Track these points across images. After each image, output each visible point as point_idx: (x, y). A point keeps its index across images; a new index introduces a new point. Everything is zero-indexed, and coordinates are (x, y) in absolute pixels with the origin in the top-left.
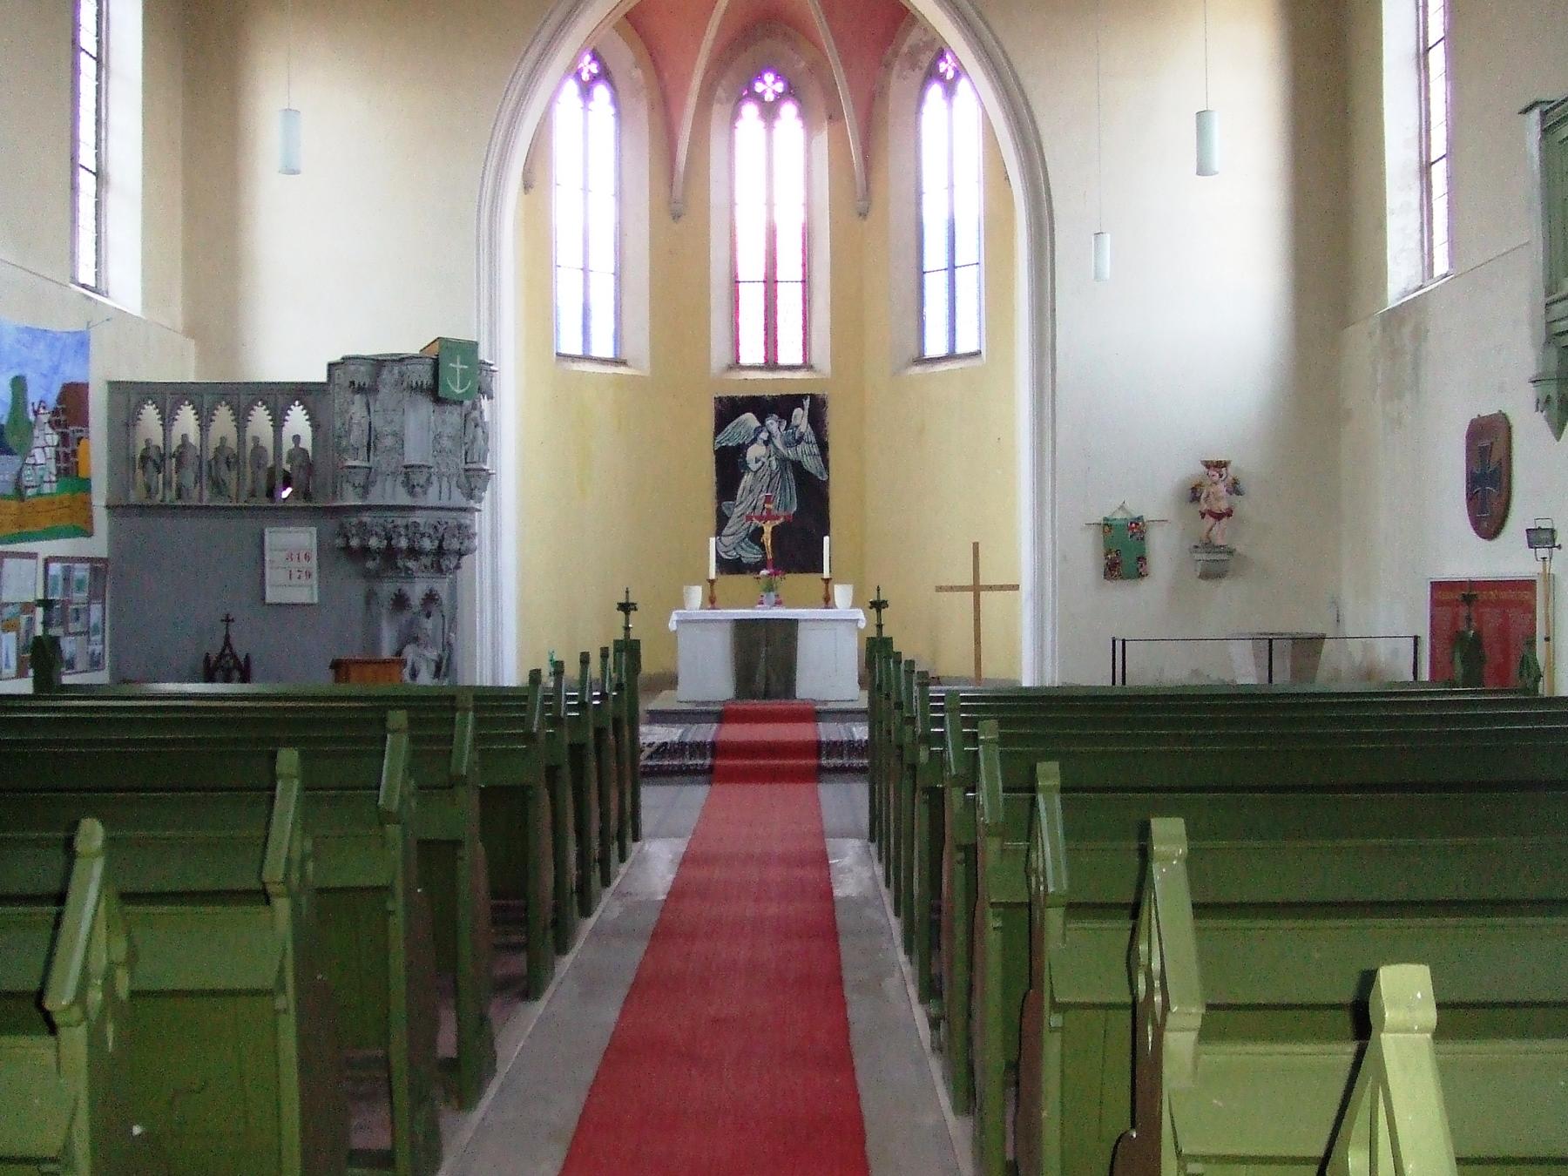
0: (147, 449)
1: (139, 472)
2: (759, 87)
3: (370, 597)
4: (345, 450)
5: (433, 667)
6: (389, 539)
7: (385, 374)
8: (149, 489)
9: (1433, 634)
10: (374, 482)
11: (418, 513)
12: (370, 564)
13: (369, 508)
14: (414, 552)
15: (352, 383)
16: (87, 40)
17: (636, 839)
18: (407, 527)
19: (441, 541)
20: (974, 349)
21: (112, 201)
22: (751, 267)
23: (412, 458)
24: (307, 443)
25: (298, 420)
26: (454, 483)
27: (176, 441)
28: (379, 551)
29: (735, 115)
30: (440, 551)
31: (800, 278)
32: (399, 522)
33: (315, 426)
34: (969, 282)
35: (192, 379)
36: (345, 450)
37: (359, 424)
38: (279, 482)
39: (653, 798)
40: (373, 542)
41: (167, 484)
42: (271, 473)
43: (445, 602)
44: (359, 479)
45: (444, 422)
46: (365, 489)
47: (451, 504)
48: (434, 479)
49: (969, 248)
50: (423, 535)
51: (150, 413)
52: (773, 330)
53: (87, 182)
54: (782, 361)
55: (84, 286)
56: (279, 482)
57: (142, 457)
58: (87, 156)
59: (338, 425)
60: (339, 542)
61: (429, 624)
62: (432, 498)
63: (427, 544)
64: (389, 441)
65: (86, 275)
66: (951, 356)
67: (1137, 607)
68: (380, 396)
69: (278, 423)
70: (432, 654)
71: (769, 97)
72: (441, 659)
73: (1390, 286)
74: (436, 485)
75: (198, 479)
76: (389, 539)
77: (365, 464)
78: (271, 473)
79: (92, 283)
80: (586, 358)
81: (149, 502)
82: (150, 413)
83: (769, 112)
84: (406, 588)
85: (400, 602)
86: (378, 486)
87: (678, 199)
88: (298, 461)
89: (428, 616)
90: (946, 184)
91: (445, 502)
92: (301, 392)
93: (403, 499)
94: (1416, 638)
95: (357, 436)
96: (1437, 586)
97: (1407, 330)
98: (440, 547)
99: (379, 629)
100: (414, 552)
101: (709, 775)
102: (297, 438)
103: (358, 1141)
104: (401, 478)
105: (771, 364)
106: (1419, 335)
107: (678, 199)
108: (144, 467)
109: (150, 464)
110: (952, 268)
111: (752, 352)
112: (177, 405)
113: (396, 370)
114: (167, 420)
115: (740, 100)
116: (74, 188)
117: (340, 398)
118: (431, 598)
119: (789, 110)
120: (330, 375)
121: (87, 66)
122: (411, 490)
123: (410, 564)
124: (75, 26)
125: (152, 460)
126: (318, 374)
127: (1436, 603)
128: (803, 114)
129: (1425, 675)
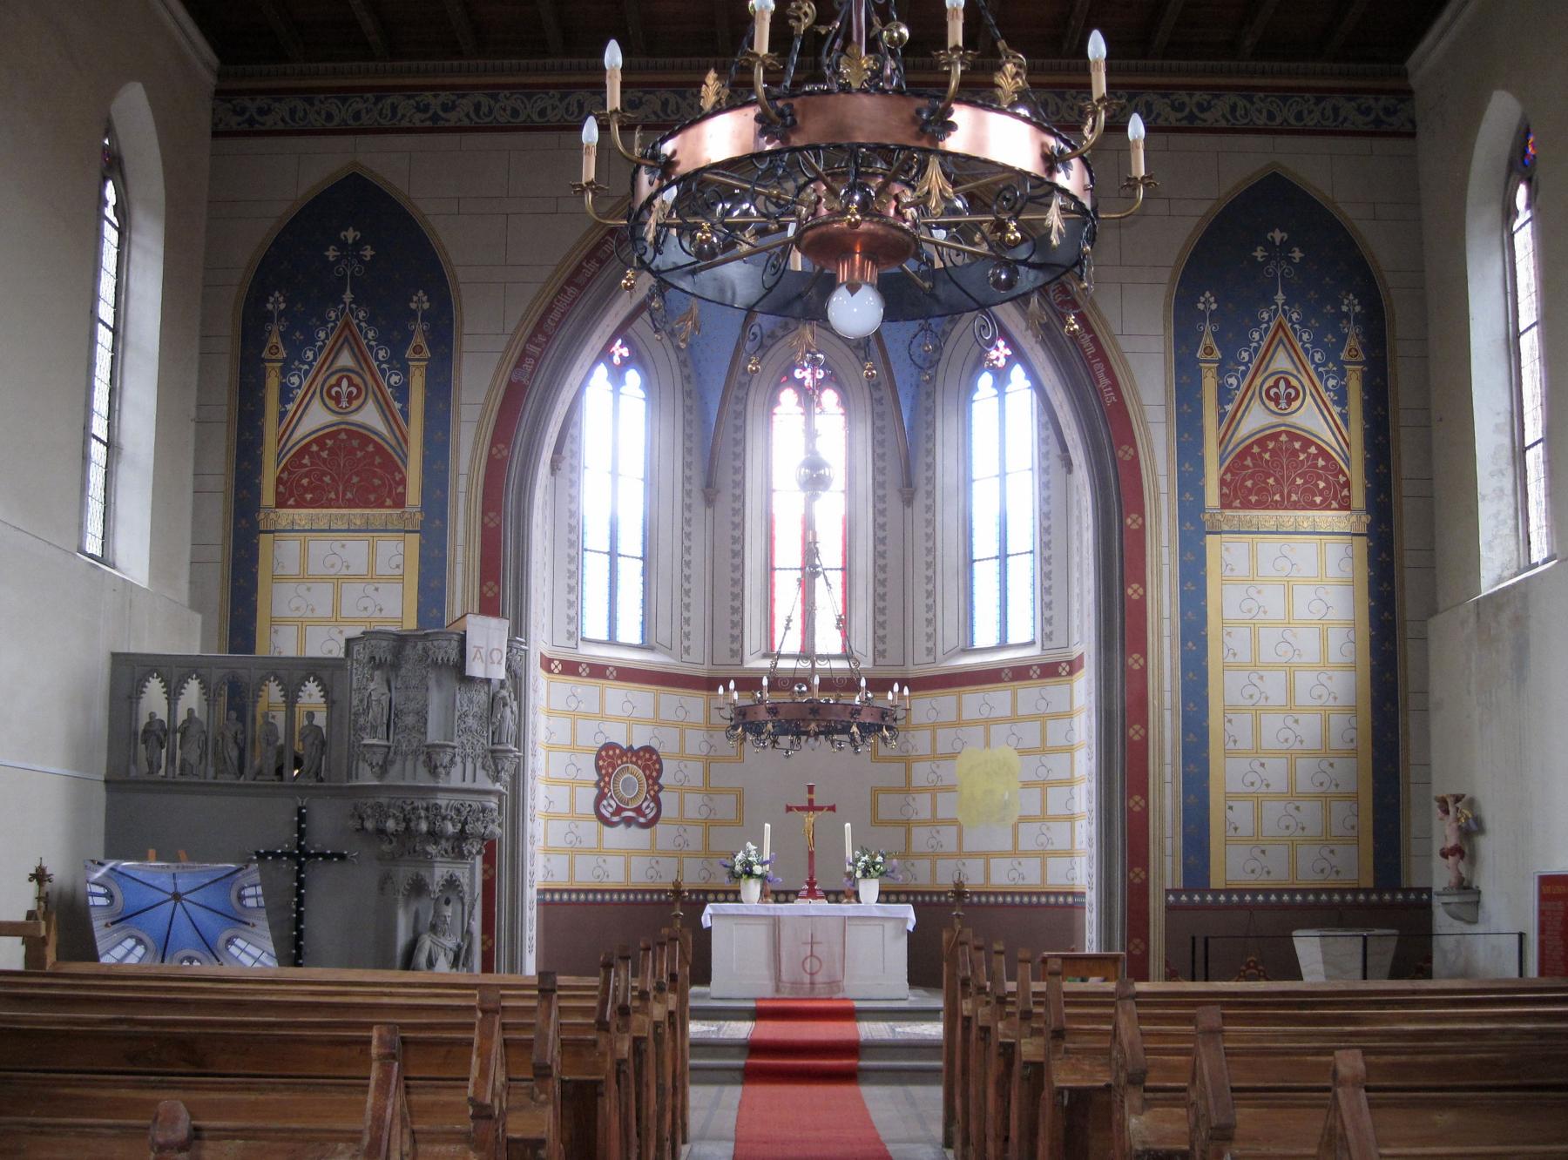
0: (149, 724)
1: (142, 747)
2: (798, 374)
3: (385, 881)
4: (363, 729)
5: (451, 956)
6: (407, 821)
7: (409, 651)
8: (150, 764)
9: (1542, 929)
10: (393, 762)
11: (440, 795)
12: (386, 847)
13: (388, 788)
14: (434, 835)
15: (373, 658)
16: (106, 312)
17: (684, 1142)
18: (427, 809)
19: (465, 823)
20: (1028, 639)
21: (124, 474)
22: (788, 553)
23: (433, 736)
24: (320, 720)
25: (312, 694)
26: (479, 765)
27: (182, 716)
28: (396, 834)
29: (773, 401)
30: (462, 836)
31: (777, 574)
32: (418, 803)
33: (330, 702)
34: (1023, 572)
35: (197, 653)
36: (363, 729)
37: (379, 701)
38: (288, 761)
39: (699, 1097)
40: (391, 825)
41: (171, 759)
42: (280, 752)
43: (466, 888)
44: (378, 759)
45: (471, 701)
46: (383, 769)
47: (477, 786)
48: (458, 759)
49: (1023, 535)
50: (444, 818)
51: (155, 688)
52: (807, 621)
53: (98, 452)
54: (819, 650)
55: (91, 556)
56: (288, 761)
57: (145, 732)
58: (99, 427)
59: (355, 702)
60: (356, 824)
61: (448, 911)
62: (455, 780)
63: (450, 828)
64: (410, 720)
65: (93, 546)
66: (1003, 645)
67: (1253, 876)
68: (403, 672)
69: (291, 698)
70: (450, 942)
71: (808, 382)
72: (459, 947)
73: (1483, 573)
74: (459, 766)
75: (203, 756)
76: (407, 821)
77: (384, 743)
78: (280, 752)
79: (99, 554)
80: (612, 641)
81: (152, 778)
82: (155, 688)
83: (808, 398)
84: (423, 872)
85: (418, 888)
86: (397, 767)
87: (906, 475)
88: (310, 740)
89: (447, 902)
90: (621, 480)
91: (468, 784)
92: (317, 669)
93: (424, 780)
94: (1521, 936)
95: (377, 713)
96: (1545, 881)
97: (1506, 616)
98: (462, 830)
99: (395, 915)
100: (434, 835)
101: (751, 1076)
102: (311, 715)
103: (1020, 956)
104: (422, 758)
105: (807, 653)
106: (1520, 621)
107: (906, 475)
108: (145, 742)
109: (154, 738)
110: (1003, 557)
111: (790, 642)
112: (183, 680)
113: (420, 646)
114: (173, 695)
115: (777, 387)
116: (86, 458)
117: (358, 674)
118: (451, 884)
119: (830, 397)
120: (348, 651)
121: (104, 337)
122: (433, 770)
123: (431, 849)
124: (95, 297)
125: (157, 734)
126: (335, 650)
127: (1543, 898)
128: (845, 401)
129: (1532, 970)
